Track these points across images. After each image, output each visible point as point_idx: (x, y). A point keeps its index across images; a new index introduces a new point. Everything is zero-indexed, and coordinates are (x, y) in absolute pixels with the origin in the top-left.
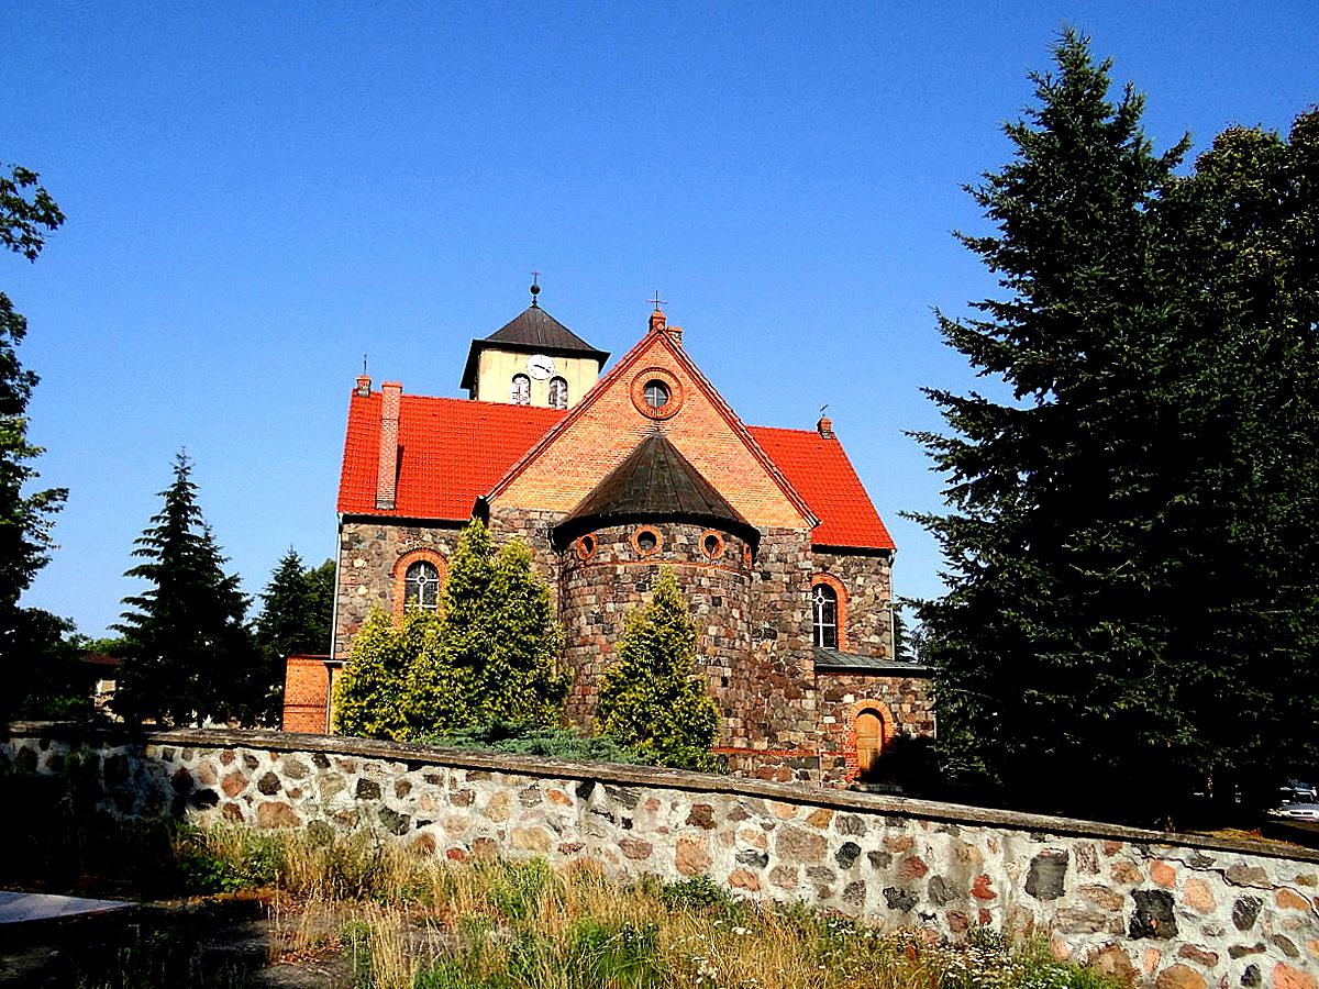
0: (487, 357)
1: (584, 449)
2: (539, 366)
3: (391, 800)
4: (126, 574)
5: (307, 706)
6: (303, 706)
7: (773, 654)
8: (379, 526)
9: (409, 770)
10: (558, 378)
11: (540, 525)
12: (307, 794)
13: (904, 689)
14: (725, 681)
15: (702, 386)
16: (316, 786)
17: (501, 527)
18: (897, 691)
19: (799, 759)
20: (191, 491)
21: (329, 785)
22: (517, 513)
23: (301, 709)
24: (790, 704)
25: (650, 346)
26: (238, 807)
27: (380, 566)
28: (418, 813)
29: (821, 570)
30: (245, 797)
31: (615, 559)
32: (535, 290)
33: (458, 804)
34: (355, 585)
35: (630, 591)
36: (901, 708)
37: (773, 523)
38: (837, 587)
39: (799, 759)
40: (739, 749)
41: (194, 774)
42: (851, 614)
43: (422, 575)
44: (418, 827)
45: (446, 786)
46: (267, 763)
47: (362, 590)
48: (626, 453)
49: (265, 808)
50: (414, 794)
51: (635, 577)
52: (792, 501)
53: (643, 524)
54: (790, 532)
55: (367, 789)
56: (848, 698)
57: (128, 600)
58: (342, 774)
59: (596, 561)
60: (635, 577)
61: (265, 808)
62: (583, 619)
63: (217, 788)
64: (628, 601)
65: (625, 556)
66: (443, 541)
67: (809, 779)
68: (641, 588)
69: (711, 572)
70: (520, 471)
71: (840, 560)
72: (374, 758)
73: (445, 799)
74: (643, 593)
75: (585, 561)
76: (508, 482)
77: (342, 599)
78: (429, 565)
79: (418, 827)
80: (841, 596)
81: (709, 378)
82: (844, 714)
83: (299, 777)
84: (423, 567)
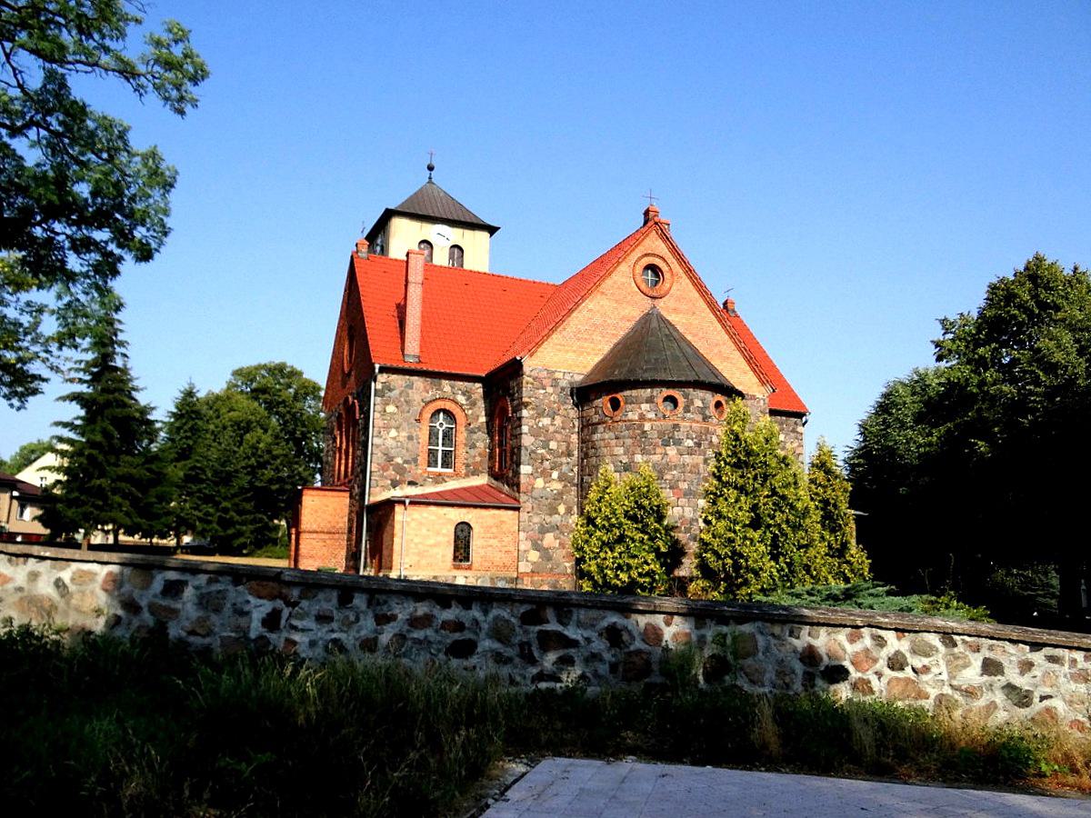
0: (399, 226)
1: (598, 320)
2: (442, 237)
3: (1012, 675)
4: (58, 399)
5: (321, 532)
6: (317, 532)
8: (408, 377)
9: (1031, 651)
10: (456, 246)
11: (563, 383)
12: (935, 670)
15: (689, 272)
16: (942, 662)
17: (532, 384)
20: (120, 327)
21: (956, 663)
22: (545, 372)
23: (315, 535)
25: (647, 235)
26: (870, 682)
27: (409, 412)
28: (1039, 688)
30: (876, 673)
31: (642, 417)
32: (431, 168)
33: (1076, 681)
34: (387, 428)
35: (656, 445)
41: (822, 651)
43: (441, 421)
44: (1040, 701)
45: (1067, 665)
46: (894, 644)
47: (393, 433)
48: (630, 325)
49: (894, 683)
50: (1037, 672)
51: (661, 434)
52: (755, 371)
53: (667, 388)
55: (990, 667)
57: (57, 424)
58: (967, 653)
59: (624, 418)
60: (661, 434)
61: (894, 683)
62: (611, 467)
63: (847, 664)
64: (655, 454)
65: (651, 415)
66: (460, 392)
68: (666, 444)
70: (548, 336)
72: (998, 639)
73: (1065, 676)
74: (668, 448)
75: (612, 418)
76: (538, 345)
77: (376, 441)
78: (447, 412)
79: (1040, 701)
81: (693, 264)
83: (927, 655)
84: (441, 415)
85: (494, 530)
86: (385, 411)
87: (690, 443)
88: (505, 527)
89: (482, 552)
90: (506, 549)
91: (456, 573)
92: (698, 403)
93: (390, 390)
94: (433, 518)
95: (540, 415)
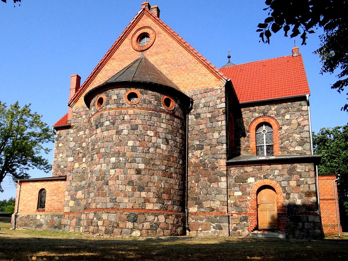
7: (201, 158)
8: (67, 130)
13: (291, 172)
14: (138, 172)
17: (76, 116)
18: (285, 173)
19: (216, 217)
24: (211, 186)
27: (67, 145)
29: (262, 115)
32: (229, 57)
36: (289, 184)
37: (201, 87)
38: (272, 122)
39: (216, 217)
40: (150, 210)
42: (282, 136)
54: (212, 90)
56: (251, 180)
67: (221, 229)
69: (131, 111)
71: (274, 108)
80: (275, 127)
82: (248, 190)
85: (55, 192)
86: (58, 146)
87: (107, 123)
88: (60, 189)
89: (50, 203)
90: (60, 200)
91: (38, 213)
92: (115, 97)
93: (61, 137)
94: (31, 188)
95: (79, 131)
